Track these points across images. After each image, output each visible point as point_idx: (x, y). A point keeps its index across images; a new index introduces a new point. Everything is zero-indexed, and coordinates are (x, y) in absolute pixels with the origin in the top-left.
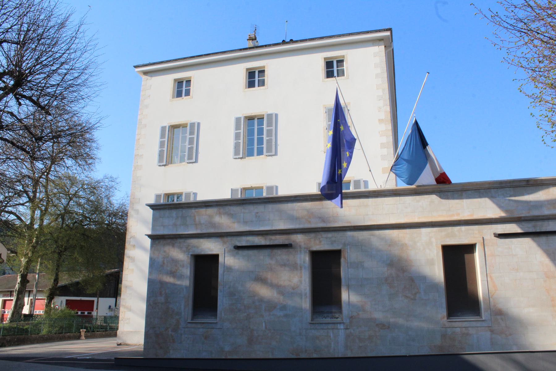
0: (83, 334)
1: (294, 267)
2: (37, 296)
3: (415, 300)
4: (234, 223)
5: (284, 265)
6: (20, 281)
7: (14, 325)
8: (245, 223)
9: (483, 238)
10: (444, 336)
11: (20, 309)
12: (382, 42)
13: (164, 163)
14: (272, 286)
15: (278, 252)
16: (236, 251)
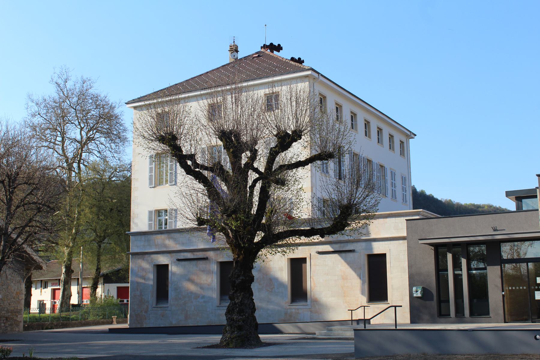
0: (114, 320)
1: (209, 272)
2: (83, 284)
3: (272, 292)
4: (177, 244)
5: (203, 271)
6: (65, 272)
7: (64, 314)
8: (183, 244)
9: (310, 254)
10: (286, 314)
11: (68, 300)
12: (307, 79)
13: (153, 186)
14: (196, 284)
15: (201, 262)
16: (178, 262)
